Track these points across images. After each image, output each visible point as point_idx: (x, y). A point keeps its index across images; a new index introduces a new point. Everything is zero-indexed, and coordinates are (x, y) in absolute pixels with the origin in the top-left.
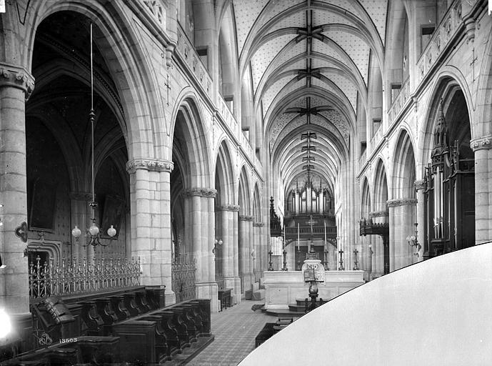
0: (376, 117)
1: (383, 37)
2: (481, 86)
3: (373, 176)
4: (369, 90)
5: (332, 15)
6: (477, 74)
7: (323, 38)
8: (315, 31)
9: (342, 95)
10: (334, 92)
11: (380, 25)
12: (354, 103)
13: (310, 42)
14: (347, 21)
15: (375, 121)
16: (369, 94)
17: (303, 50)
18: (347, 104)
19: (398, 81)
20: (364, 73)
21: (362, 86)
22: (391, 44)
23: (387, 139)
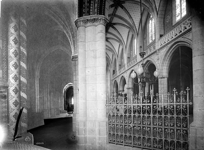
0: (120, 64)
1: (126, 45)
2: (160, 65)
3: (119, 80)
4: (118, 57)
5: (112, 36)
6: (159, 62)
7: (114, 28)
8: (111, 24)
9: (122, 39)
10: (119, 37)
11: (125, 41)
12: (111, 59)
13: (116, 8)
14: (124, 22)
15: (129, 58)
16: (118, 58)
17: (111, 13)
18: (109, 59)
19: (129, 56)
20: (117, 52)
21: (117, 56)
22: (128, 47)
23: (138, 63)
